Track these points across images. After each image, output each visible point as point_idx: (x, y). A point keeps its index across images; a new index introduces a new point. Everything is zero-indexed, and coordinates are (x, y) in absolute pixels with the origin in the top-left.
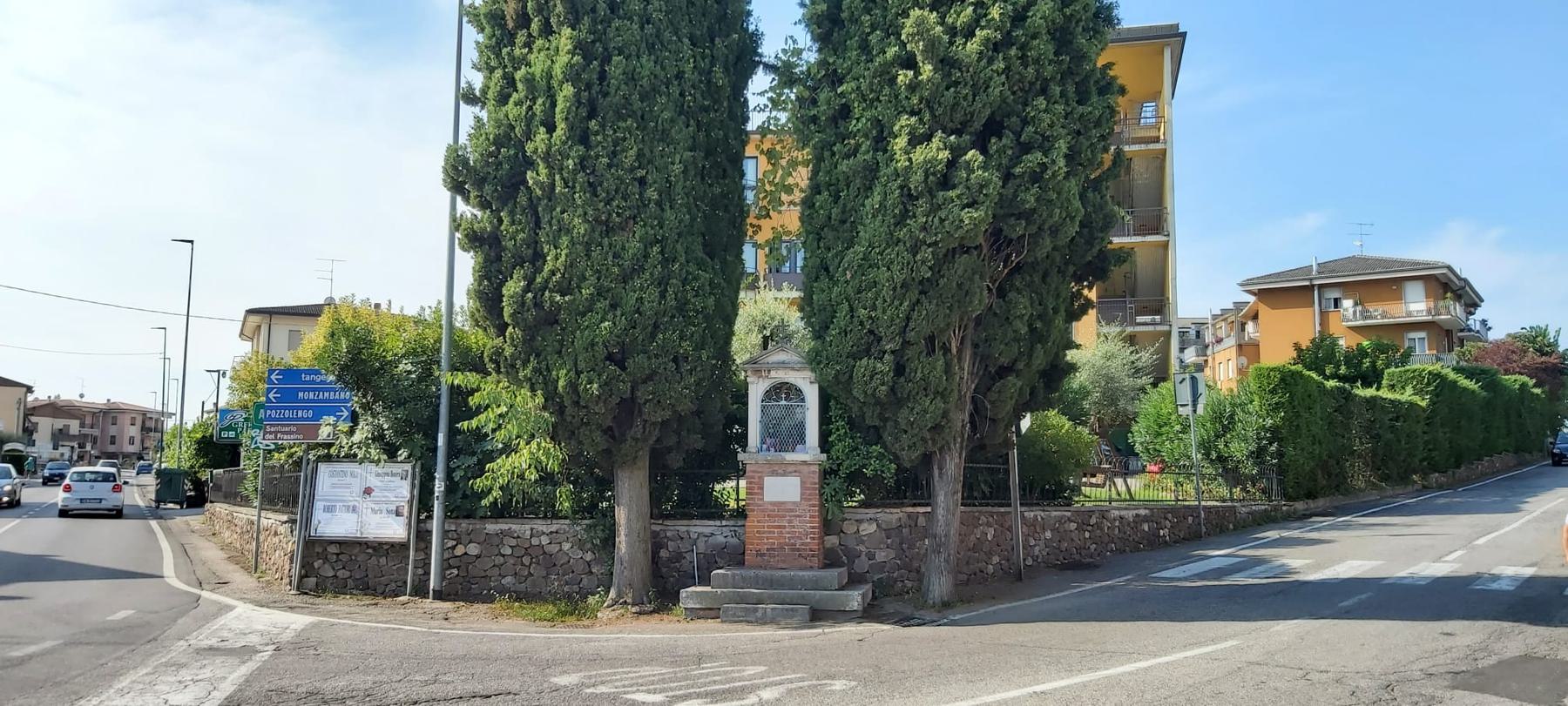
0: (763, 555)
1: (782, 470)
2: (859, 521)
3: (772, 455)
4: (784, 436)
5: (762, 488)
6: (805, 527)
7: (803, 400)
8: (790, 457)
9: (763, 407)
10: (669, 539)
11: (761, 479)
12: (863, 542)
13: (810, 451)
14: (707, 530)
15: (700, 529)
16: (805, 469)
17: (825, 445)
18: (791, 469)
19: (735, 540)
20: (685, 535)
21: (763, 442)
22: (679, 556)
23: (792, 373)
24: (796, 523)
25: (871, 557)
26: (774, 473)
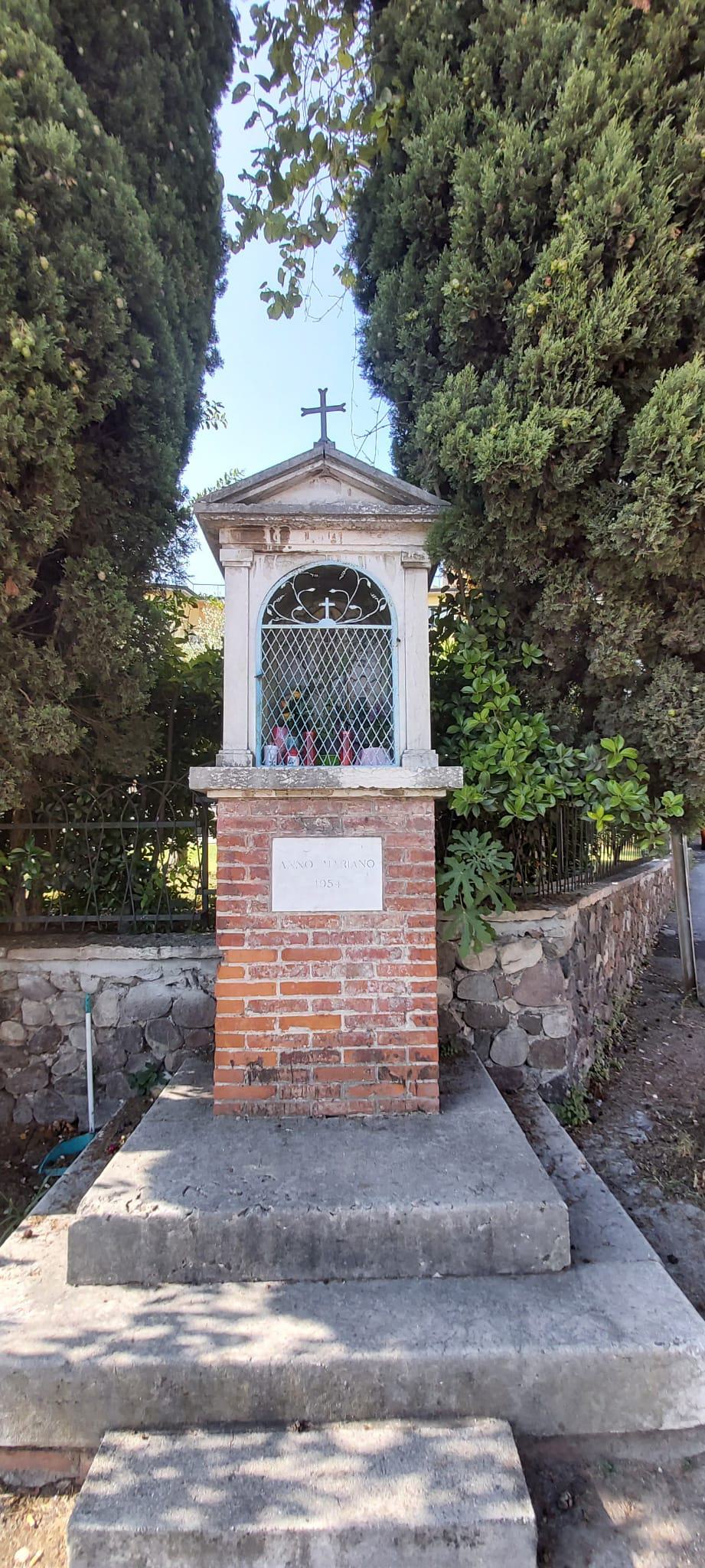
0: (267, 1076)
1: (326, 816)
2: (502, 941)
3: (294, 773)
4: (324, 723)
5: (265, 873)
6: (395, 995)
7: (385, 617)
8: (351, 777)
9: (268, 636)
10: (28, 995)
11: (262, 843)
12: (510, 992)
13: (410, 766)
14: (123, 971)
15: (103, 969)
16: (396, 813)
17: (447, 739)
18: (351, 814)
19: (194, 995)
20: (67, 984)
21: (267, 737)
22: (53, 1036)
23: (351, 539)
24: (369, 973)
25: (532, 1025)
26: (300, 827)
